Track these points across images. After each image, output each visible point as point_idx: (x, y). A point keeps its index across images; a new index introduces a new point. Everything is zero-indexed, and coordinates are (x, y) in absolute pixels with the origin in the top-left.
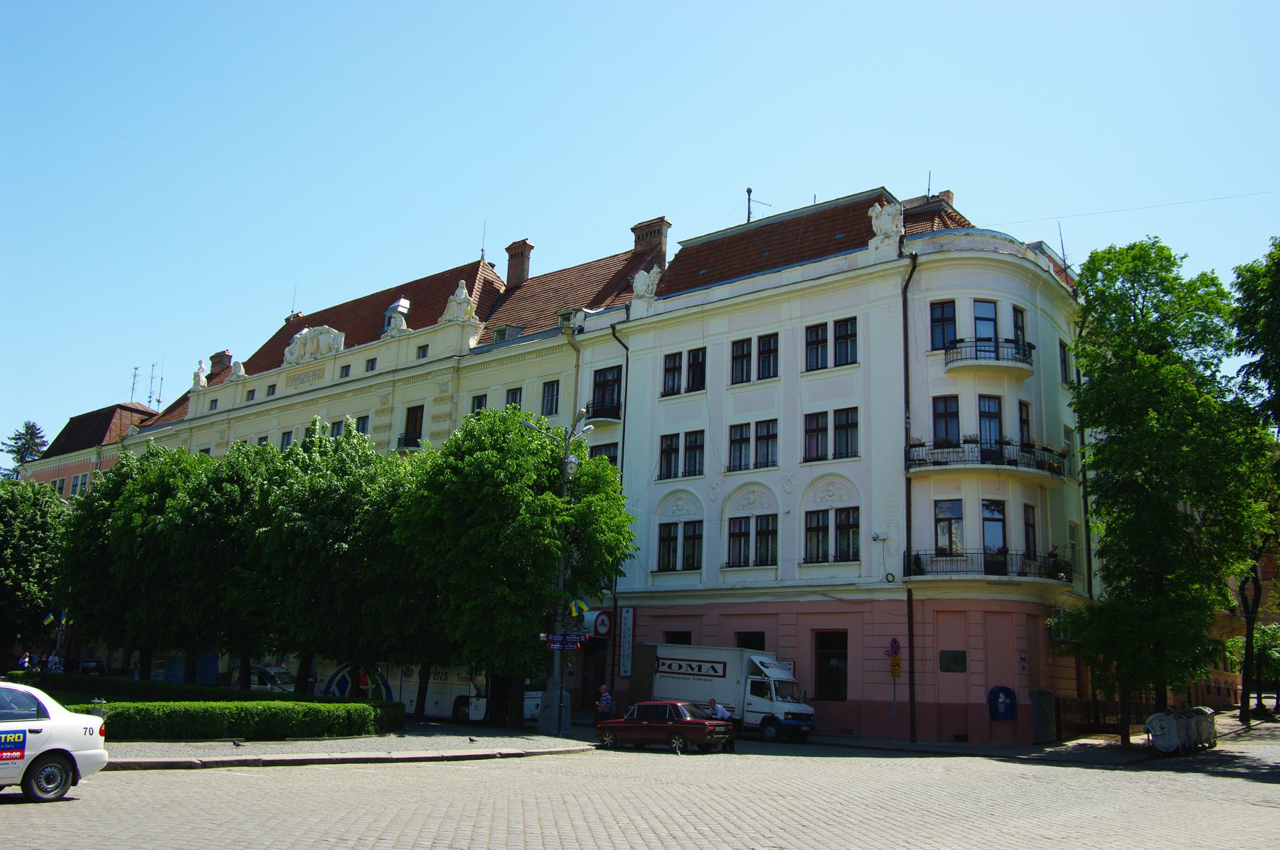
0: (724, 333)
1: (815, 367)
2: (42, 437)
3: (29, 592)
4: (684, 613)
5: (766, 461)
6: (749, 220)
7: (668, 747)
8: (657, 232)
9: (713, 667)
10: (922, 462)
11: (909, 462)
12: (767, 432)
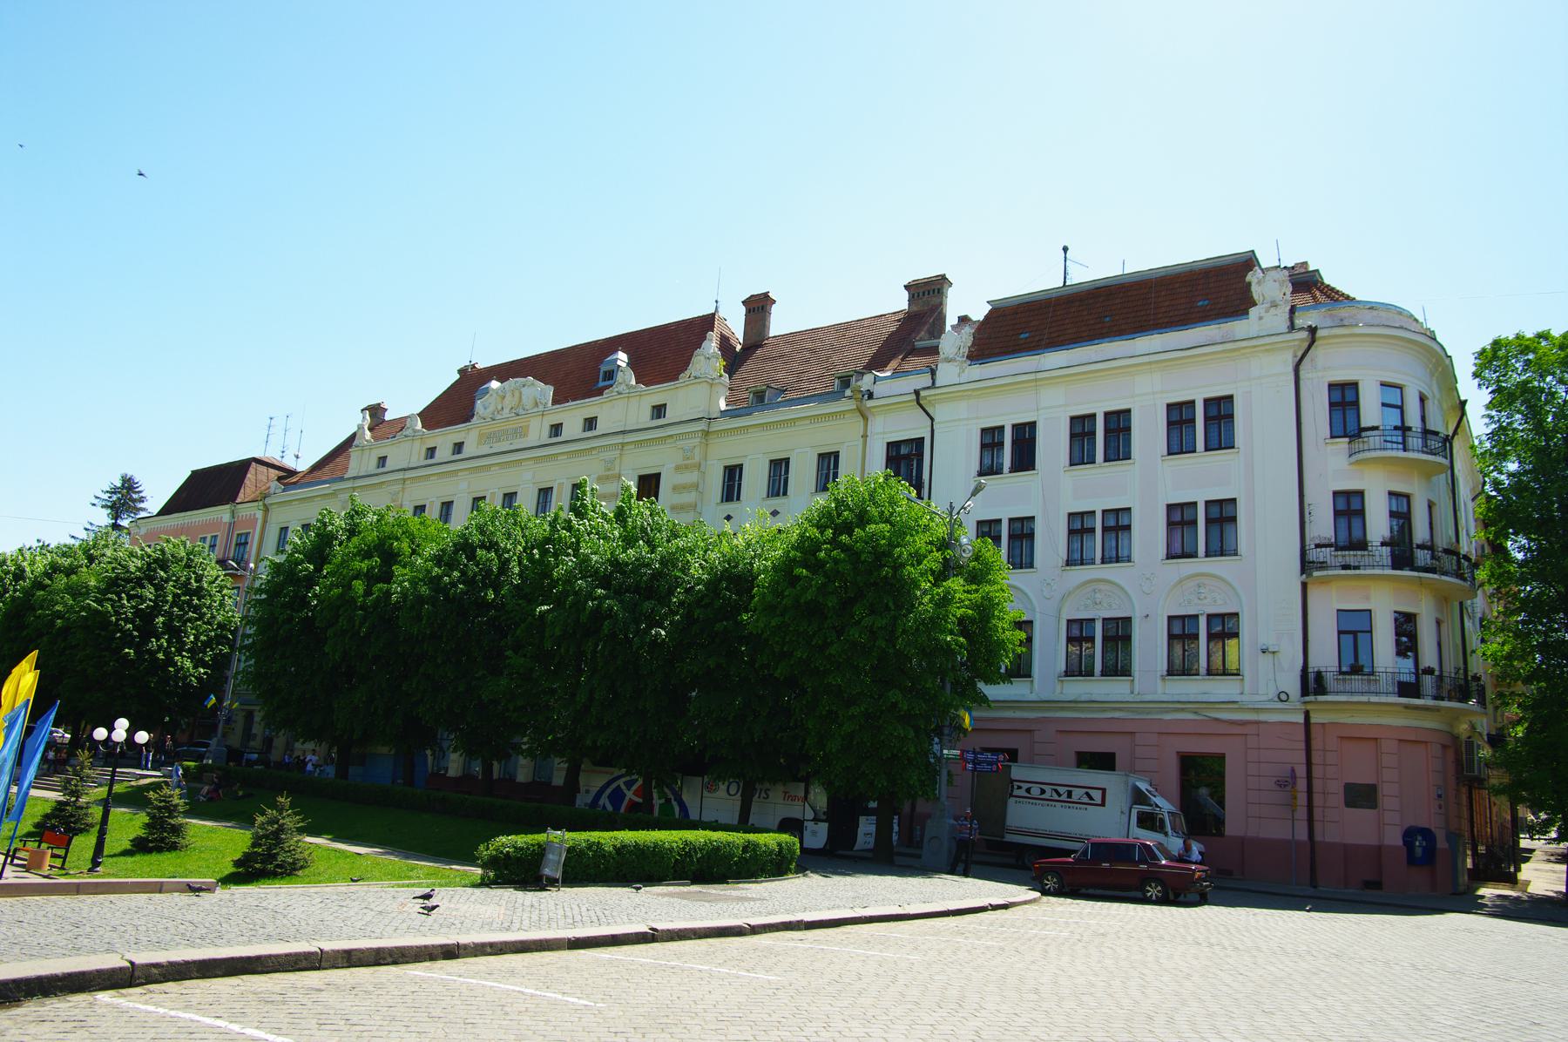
0: (1060, 406)
1: (1217, 446)
2: (140, 492)
3: (182, 668)
5: (1115, 557)
6: (1065, 282)
7: (1139, 894)
8: (936, 291)
9: (1087, 794)
10: (1322, 566)
11: (1306, 566)
12: (1118, 523)
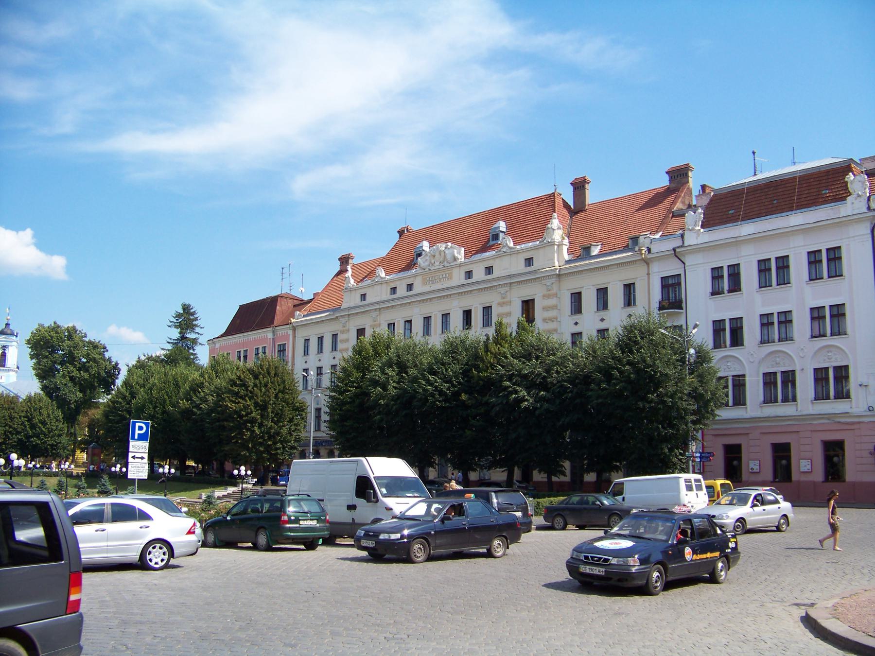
4: (742, 432)
5: (786, 338)
12: (785, 319)
